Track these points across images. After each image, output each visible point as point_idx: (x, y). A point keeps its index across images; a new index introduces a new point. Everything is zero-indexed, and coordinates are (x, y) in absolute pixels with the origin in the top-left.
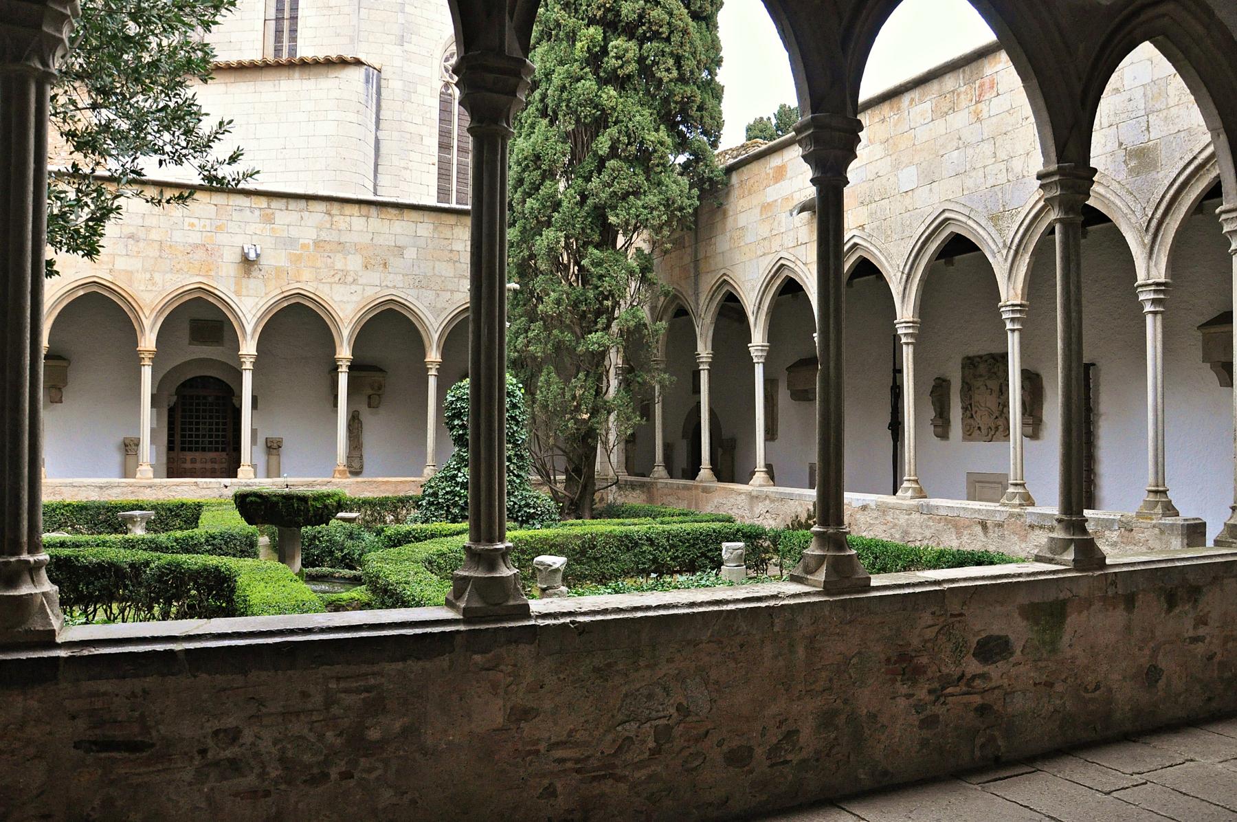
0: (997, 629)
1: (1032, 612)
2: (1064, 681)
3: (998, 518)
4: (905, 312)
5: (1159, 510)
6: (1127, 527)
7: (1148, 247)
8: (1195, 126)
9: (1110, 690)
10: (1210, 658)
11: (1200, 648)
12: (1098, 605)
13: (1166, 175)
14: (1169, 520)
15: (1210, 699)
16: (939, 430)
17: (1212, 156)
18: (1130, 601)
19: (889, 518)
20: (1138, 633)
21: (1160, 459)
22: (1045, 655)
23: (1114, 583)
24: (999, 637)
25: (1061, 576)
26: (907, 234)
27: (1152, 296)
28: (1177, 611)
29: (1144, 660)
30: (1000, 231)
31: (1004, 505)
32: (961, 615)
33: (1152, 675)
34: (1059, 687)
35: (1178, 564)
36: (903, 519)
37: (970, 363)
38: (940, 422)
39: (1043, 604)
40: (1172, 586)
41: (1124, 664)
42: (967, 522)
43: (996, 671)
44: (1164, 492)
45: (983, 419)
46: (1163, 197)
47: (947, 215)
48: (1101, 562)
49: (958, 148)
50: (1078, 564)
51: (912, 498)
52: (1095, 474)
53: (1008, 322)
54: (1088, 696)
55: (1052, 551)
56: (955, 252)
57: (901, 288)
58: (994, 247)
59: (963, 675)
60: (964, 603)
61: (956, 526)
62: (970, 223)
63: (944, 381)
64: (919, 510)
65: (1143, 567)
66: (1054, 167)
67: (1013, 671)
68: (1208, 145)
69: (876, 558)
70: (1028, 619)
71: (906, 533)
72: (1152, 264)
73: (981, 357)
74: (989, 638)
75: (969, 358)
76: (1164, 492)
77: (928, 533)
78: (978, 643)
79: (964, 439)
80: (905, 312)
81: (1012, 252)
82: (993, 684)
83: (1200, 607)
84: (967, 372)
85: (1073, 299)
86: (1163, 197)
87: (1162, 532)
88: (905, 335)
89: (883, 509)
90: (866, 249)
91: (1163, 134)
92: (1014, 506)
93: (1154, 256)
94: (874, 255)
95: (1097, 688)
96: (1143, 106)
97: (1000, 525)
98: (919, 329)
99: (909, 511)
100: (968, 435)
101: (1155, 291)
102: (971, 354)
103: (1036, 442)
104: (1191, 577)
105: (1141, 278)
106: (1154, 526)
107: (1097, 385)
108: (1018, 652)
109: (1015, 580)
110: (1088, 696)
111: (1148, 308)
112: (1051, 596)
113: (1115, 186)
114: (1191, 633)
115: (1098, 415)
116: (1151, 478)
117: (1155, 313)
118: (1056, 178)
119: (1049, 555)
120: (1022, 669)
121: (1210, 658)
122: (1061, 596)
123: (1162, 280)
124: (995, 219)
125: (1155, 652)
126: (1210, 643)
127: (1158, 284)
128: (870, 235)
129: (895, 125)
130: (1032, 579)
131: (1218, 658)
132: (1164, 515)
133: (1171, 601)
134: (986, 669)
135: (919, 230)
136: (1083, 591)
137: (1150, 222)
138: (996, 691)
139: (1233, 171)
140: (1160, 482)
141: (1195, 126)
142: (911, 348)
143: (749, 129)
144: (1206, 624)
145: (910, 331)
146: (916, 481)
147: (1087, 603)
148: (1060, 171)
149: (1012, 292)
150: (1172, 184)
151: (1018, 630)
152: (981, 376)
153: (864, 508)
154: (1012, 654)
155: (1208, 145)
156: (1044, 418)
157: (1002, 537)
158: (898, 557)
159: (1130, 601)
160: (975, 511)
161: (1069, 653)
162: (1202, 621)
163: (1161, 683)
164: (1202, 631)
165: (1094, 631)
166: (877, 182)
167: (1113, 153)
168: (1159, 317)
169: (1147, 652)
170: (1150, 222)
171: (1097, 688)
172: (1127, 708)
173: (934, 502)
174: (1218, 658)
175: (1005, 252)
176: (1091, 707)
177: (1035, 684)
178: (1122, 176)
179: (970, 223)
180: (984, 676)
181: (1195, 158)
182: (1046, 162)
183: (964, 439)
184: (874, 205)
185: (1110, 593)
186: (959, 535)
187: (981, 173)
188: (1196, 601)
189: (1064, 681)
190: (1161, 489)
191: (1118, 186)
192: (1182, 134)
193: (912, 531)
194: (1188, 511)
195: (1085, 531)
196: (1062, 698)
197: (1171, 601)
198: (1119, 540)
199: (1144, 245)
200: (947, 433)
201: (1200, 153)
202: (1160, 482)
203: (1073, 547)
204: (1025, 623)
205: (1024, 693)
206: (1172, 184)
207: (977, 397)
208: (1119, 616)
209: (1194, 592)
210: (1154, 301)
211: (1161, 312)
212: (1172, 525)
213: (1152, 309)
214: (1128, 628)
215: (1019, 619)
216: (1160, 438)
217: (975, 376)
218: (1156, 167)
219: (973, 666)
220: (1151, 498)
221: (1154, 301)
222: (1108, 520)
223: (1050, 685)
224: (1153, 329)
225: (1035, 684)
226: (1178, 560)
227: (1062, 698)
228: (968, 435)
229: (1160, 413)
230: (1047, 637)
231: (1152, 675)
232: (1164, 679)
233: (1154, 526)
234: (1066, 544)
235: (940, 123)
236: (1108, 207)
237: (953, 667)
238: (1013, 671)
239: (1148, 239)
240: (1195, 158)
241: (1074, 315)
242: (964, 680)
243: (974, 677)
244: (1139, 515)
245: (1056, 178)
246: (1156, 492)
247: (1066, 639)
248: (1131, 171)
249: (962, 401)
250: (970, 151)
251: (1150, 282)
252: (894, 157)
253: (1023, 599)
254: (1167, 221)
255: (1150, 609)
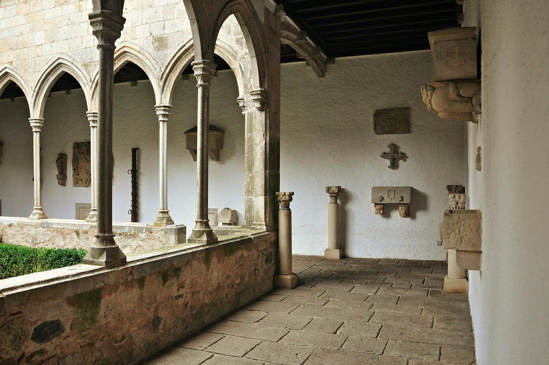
0: (49, 317)
1: (76, 301)
2: (102, 340)
3: (85, 228)
4: (36, 114)
5: (164, 221)
6: (150, 231)
7: (162, 87)
8: (185, 30)
9: (131, 337)
10: (186, 305)
11: (181, 301)
12: (122, 288)
13: (171, 52)
14: (169, 227)
15: (186, 327)
16: (61, 181)
17: (192, 45)
18: (141, 282)
19: (25, 231)
20: (147, 300)
21: (165, 196)
22: (87, 326)
23: (131, 273)
24: (52, 322)
25: (97, 273)
26: (37, 69)
27: (162, 112)
28: (168, 283)
29: (150, 315)
30: (88, 73)
31: (88, 221)
32: (19, 313)
33: (156, 322)
34: (98, 345)
35: (168, 256)
36: (33, 231)
37: (77, 146)
38: (61, 177)
39: (85, 295)
40: (165, 269)
41: (139, 320)
42: (68, 231)
43: (49, 346)
44: (167, 212)
45: (83, 175)
46: (169, 63)
47: (60, 61)
48: (124, 261)
49: (68, 25)
50: (108, 264)
51: (38, 219)
52: (138, 203)
53: (91, 122)
54: (117, 345)
55: (93, 257)
56: (64, 84)
57: (33, 100)
58: (84, 80)
59: (23, 355)
60: (21, 304)
61: (62, 234)
62: (73, 66)
63: (64, 155)
64: (42, 225)
65: (149, 261)
66: (99, 11)
67: (64, 343)
68: (190, 40)
69: (11, 256)
70: (73, 305)
71: (35, 239)
72: (163, 96)
73: (83, 143)
74: (44, 324)
75: (77, 143)
76: (167, 212)
77: (47, 238)
78: (35, 330)
79: (74, 186)
80: (36, 114)
81: (94, 85)
82: (49, 355)
83: (180, 278)
84: (75, 150)
85: (107, 96)
86: (169, 63)
87: (166, 233)
88: (35, 127)
89: (22, 226)
90: (13, 76)
91: (171, 31)
92: (93, 222)
93: (164, 92)
94: (18, 80)
95: (123, 338)
96: (162, 16)
97: (86, 232)
98: (44, 124)
99: (36, 226)
100: (76, 183)
101: (164, 110)
102: (78, 141)
103: (63, 188)
104: (175, 263)
105: (158, 104)
106: (162, 230)
107: (139, 159)
108: (68, 328)
109: (63, 281)
110: (117, 345)
111: (161, 118)
112: (91, 287)
113: (147, 55)
114: (176, 294)
115: (140, 174)
116: (161, 206)
117: (164, 121)
118: (100, 19)
119: (91, 259)
120: (71, 339)
121: (186, 305)
122: (97, 286)
123: (168, 105)
124: (86, 66)
125: (157, 309)
126: (186, 297)
127: (165, 107)
128: (15, 68)
129: (33, 6)
130: (76, 278)
131: (190, 304)
132: (167, 224)
133: (165, 278)
134: (43, 346)
135: (44, 68)
136: (111, 281)
137: (163, 75)
138: (51, 360)
139: (199, 43)
140: (165, 207)
141: (185, 30)
142: (38, 134)
143: (235, 211)
144: (183, 287)
145: (38, 125)
146: (41, 209)
147: (115, 288)
148: (102, 14)
149: (93, 106)
150: (174, 57)
151: (66, 315)
152: (83, 153)
153: (10, 225)
154: (63, 331)
155: (190, 40)
156: (114, 175)
157: (87, 239)
158: (24, 255)
159: (141, 282)
160: (73, 225)
161: (103, 321)
162: (181, 286)
163: (161, 326)
164: (181, 292)
165: (121, 302)
166: (21, 37)
167: (147, 38)
168: (166, 123)
169: (152, 309)
170: (163, 75)
171: (123, 338)
172: (142, 345)
173: (49, 220)
174: (190, 304)
175: (90, 84)
176: (120, 351)
177: (81, 347)
178: (151, 50)
179: (73, 66)
180: (41, 352)
181: (184, 45)
182: (95, 8)
183: (74, 186)
184: (19, 51)
185: (129, 280)
186: (64, 238)
187: (80, 40)
188: (178, 276)
189: (102, 340)
190: (165, 211)
191: (149, 55)
192: (179, 33)
193: (38, 237)
194: (178, 222)
195: (113, 242)
196: (100, 351)
197: (165, 278)
198: (146, 238)
199: (160, 86)
200: (65, 183)
201: (187, 43)
202: (165, 207)
203: (105, 253)
204: (71, 309)
205: (73, 354)
206: (174, 57)
207: (81, 164)
208: (135, 292)
209: (177, 271)
210: (164, 115)
211: (167, 121)
212: (171, 229)
213: (162, 119)
214: (141, 299)
215: (67, 307)
216: (165, 185)
217: (80, 153)
218: (167, 48)
219: (32, 346)
220: (161, 215)
221: (164, 115)
222: (140, 228)
223: (92, 345)
224: (163, 129)
225: (81, 347)
226: (168, 254)
227: (100, 351)
228: (76, 183)
229: (165, 172)
230: (88, 315)
231: (156, 322)
232: (162, 322)
233: (162, 230)
234: (101, 251)
235: (59, 9)
236: (144, 65)
237: (13, 353)
238: (64, 343)
239: (162, 83)
240: (184, 45)
241: (107, 106)
242: (24, 359)
243: (32, 355)
244: (156, 224)
245: (100, 19)
246: (163, 212)
247: (102, 313)
248: (155, 48)
249: (73, 166)
250: (75, 27)
251: (162, 105)
252: (31, 24)
253: (69, 293)
254: (171, 75)
255: (153, 285)
